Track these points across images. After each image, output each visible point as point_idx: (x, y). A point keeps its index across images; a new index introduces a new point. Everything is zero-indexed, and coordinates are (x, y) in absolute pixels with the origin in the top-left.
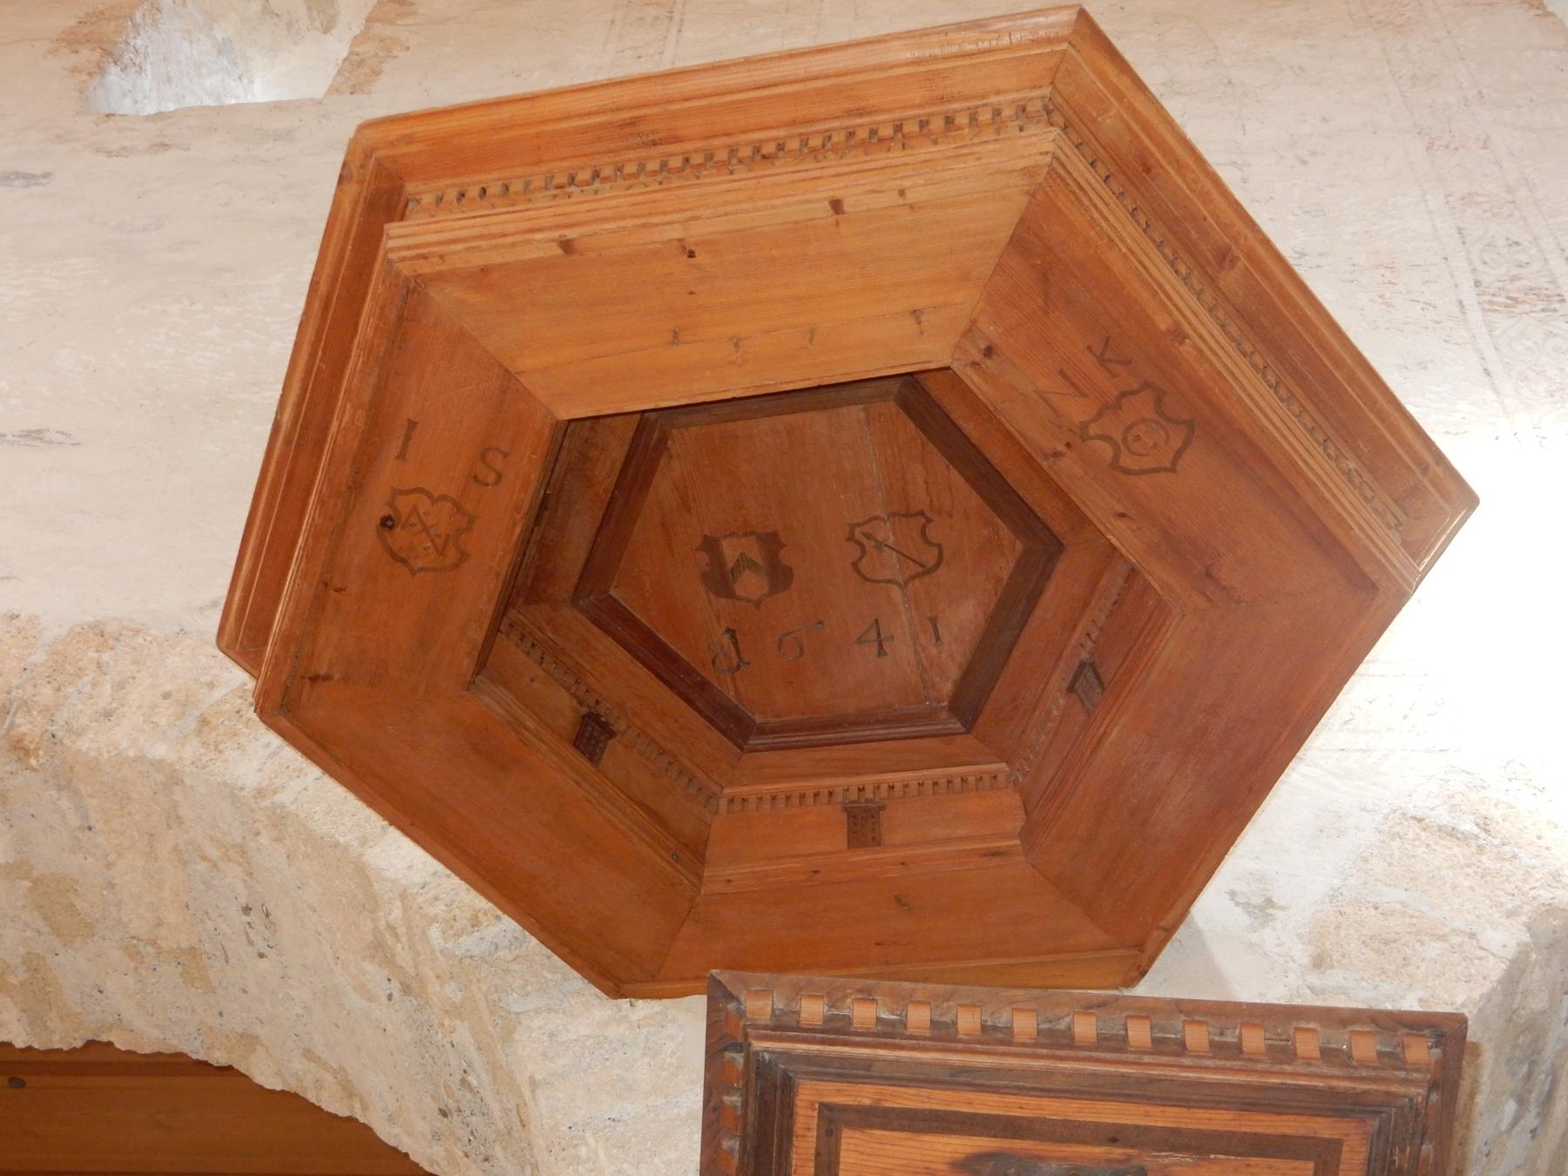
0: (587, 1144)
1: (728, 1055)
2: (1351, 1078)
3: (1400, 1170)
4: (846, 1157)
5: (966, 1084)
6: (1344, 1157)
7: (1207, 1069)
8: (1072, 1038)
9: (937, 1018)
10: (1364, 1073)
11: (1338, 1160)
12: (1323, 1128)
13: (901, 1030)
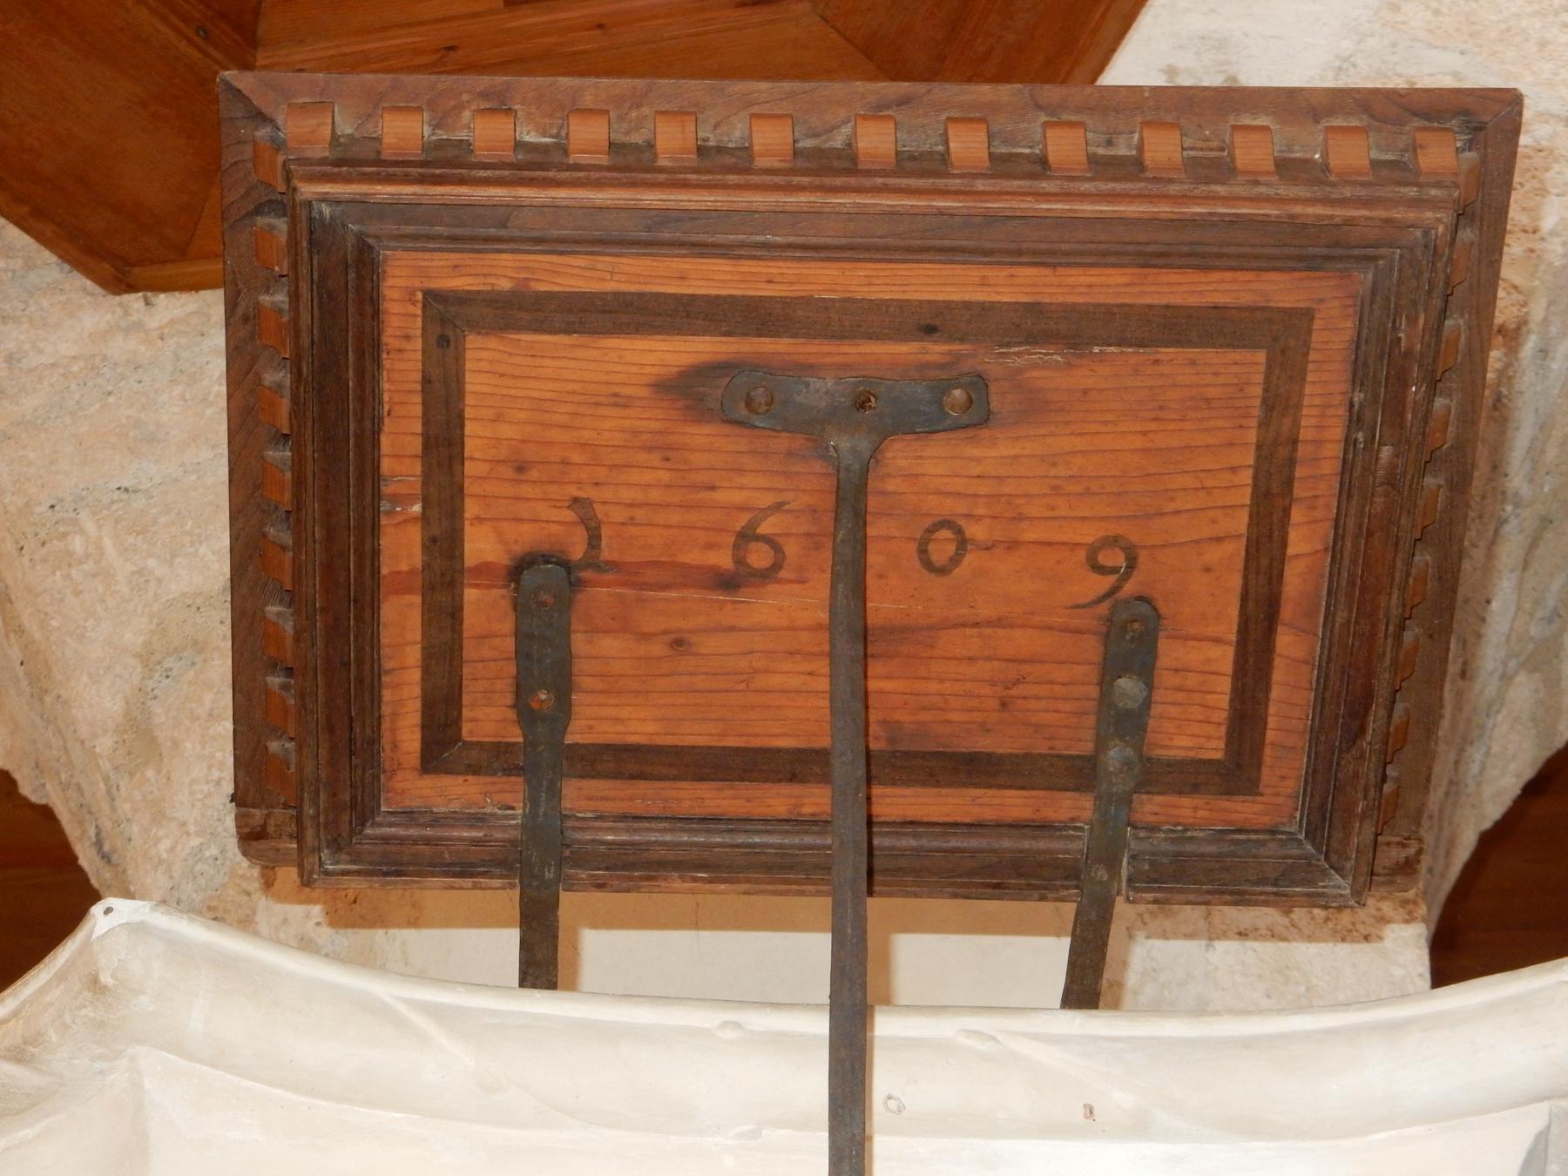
0: (82, 531)
1: (262, 221)
2: (1327, 201)
3: (1408, 353)
4: (475, 383)
5: (672, 244)
6: (1316, 338)
7: (1083, 196)
8: (854, 159)
9: (619, 137)
10: (1348, 192)
11: (1307, 344)
12: (1281, 290)
13: (556, 157)
